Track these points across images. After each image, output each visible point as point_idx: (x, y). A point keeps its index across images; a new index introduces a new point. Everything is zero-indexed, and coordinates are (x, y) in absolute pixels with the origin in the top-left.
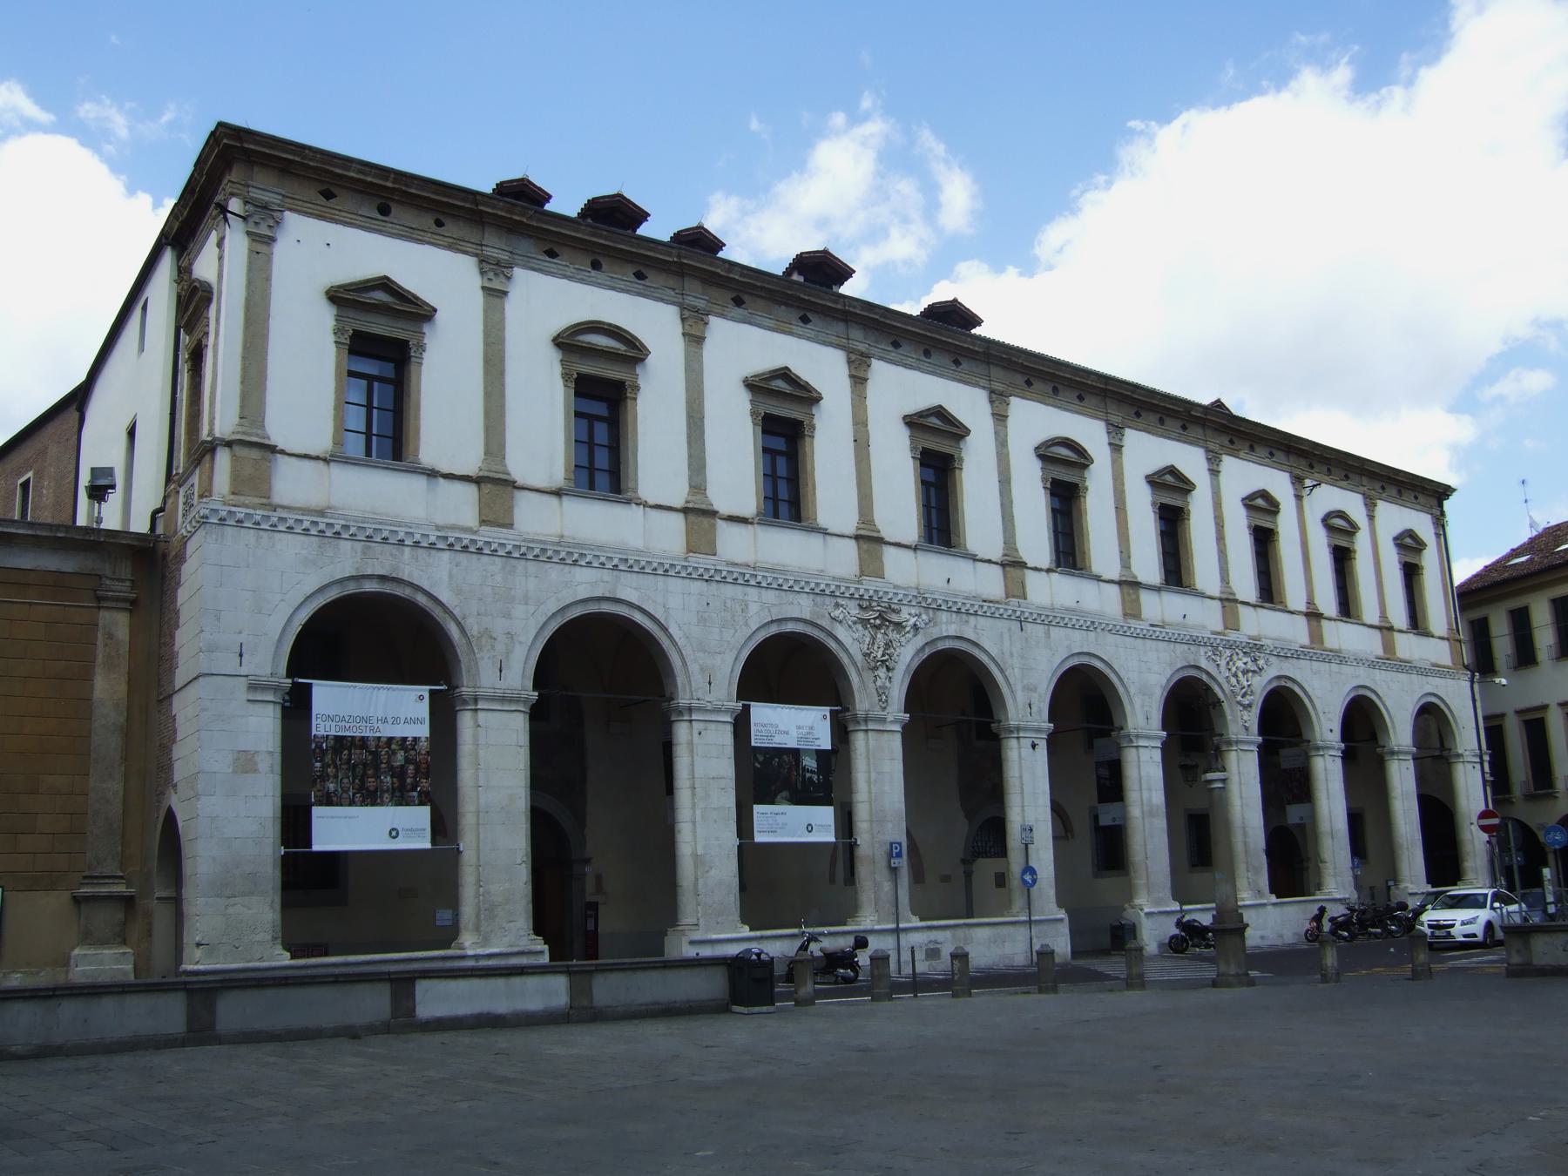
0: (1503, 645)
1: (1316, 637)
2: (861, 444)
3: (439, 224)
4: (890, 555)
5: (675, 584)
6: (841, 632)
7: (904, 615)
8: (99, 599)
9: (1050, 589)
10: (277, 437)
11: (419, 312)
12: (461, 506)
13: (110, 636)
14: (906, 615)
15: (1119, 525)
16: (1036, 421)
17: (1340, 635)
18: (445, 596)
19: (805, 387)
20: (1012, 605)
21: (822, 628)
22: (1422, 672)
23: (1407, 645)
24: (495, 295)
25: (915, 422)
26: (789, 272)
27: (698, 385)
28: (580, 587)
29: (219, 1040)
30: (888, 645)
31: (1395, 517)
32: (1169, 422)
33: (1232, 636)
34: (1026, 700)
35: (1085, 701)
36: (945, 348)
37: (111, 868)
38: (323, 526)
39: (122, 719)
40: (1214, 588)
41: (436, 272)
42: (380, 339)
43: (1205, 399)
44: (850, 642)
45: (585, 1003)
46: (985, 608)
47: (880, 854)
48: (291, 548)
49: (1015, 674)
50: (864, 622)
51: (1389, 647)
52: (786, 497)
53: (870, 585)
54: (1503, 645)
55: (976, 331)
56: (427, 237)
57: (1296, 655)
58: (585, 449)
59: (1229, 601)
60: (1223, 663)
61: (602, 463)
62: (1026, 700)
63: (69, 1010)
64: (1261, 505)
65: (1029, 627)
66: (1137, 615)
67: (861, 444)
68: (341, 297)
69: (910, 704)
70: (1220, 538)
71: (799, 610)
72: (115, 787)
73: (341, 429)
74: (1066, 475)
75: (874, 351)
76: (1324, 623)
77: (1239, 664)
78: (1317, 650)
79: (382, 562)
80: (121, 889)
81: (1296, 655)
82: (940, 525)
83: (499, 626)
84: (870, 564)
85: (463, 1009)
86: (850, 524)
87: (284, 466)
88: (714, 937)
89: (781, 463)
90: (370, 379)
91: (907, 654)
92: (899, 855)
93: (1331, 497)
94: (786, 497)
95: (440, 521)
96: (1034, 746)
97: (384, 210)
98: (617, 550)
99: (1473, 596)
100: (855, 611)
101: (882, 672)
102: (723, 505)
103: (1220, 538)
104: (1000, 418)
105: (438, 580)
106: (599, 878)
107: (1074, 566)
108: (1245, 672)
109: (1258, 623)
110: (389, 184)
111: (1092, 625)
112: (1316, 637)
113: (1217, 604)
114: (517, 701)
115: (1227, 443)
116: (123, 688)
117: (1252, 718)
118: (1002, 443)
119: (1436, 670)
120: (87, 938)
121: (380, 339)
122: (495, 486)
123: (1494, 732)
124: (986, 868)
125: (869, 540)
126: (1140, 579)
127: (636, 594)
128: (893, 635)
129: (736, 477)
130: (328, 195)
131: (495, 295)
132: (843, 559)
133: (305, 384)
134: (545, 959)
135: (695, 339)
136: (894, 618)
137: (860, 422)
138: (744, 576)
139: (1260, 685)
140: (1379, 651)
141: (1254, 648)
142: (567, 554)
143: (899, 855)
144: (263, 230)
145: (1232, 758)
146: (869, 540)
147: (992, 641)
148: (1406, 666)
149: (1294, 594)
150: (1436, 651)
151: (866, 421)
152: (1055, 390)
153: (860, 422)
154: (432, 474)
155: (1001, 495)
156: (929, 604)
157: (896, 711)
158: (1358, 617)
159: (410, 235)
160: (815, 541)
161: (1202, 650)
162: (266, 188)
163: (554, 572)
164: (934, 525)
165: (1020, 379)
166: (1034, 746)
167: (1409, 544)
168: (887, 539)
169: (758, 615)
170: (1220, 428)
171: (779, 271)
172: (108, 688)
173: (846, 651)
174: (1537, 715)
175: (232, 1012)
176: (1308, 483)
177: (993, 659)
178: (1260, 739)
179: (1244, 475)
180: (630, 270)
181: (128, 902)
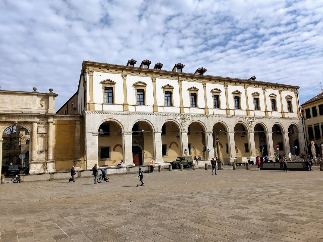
3: (116, 70)
5: (152, 116)
6: (177, 121)
7: (187, 117)
8: (75, 123)
11: (113, 83)
13: (77, 128)
16: (211, 86)
17: (275, 114)
19: (172, 87)
20: (206, 114)
21: (174, 120)
22: (291, 119)
24: (124, 79)
26: (155, 68)
30: (185, 122)
31: (285, 93)
32: (256, 85)
33: (248, 116)
34: (269, 129)
35: (277, 128)
36: (252, 83)
38: (102, 112)
39: (79, 138)
42: (109, 88)
43: (87, 61)
44: (179, 122)
45: (129, 171)
46: (202, 115)
49: (206, 125)
50: (181, 119)
55: (255, 80)
56: (98, 71)
57: (263, 118)
58: (166, 101)
60: (246, 120)
61: (142, 101)
62: (269, 129)
65: (209, 118)
66: (230, 114)
71: (171, 118)
72: (79, 147)
73: (104, 100)
75: (183, 80)
77: (250, 120)
78: (266, 117)
79: (111, 117)
83: (127, 124)
85: (113, 173)
88: (159, 163)
90: (108, 93)
91: (188, 123)
92: (187, 151)
93: (271, 91)
94: (217, 105)
95: (118, 111)
96: (210, 135)
97: (108, 70)
98: (144, 112)
100: (180, 118)
101: (184, 126)
105: (118, 118)
106: (146, 155)
107: (275, 111)
108: (251, 122)
110: (108, 66)
111: (259, 118)
113: (281, 113)
114: (130, 133)
115: (254, 85)
116: (79, 135)
121: (109, 88)
122: (206, 109)
125: (266, 111)
126: (184, 106)
127: (146, 118)
128: (186, 120)
129: (232, 105)
130: (133, 73)
131: (124, 79)
134: (134, 166)
135: (180, 84)
136: (186, 118)
139: (254, 124)
140: (281, 116)
141: (254, 117)
143: (187, 151)
144: (91, 74)
147: (202, 120)
149: (279, 108)
150: (296, 116)
152: (215, 81)
154: (117, 105)
155: (205, 98)
158: (260, 110)
161: (242, 119)
162: (91, 68)
163: (134, 116)
164: (237, 106)
166: (210, 135)
167: (289, 98)
168: (129, 104)
170: (252, 82)
171: (126, 65)
172: (77, 134)
173: (178, 123)
174: (317, 125)
176: (266, 89)
177: (146, 120)
178: (289, 132)
179: (252, 90)
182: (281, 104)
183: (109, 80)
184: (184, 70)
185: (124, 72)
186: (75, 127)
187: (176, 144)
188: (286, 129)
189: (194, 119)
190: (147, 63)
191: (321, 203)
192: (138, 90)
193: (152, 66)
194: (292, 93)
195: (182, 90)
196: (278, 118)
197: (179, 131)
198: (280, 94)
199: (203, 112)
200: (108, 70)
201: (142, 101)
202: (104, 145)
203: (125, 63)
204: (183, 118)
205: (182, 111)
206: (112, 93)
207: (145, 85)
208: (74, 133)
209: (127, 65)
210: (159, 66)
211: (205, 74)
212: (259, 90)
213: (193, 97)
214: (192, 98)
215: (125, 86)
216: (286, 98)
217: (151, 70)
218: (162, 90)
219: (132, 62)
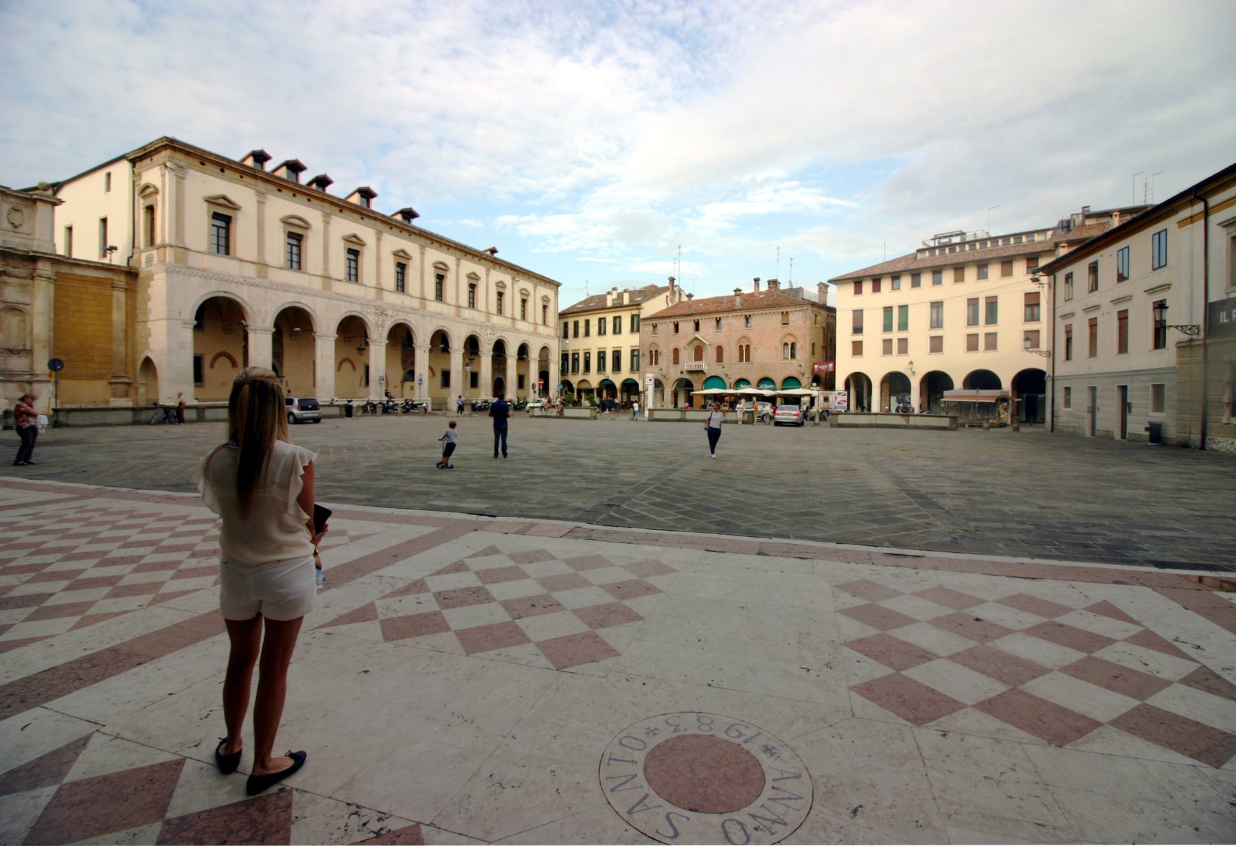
0: (571, 331)
1: (458, 315)
2: (378, 259)
4: (386, 294)
5: (318, 299)
9: (434, 306)
10: (189, 245)
11: (362, 244)
12: (251, 271)
14: (390, 312)
15: (456, 287)
16: (435, 255)
17: (521, 325)
18: (246, 299)
20: (422, 310)
23: (541, 329)
24: (261, 203)
25: (396, 254)
26: (310, 184)
27: (328, 235)
28: (288, 300)
29: (207, 421)
31: (543, 291)
37: (121, 374)
38: (205, 274)
40: (373, 283)
41: (241, 193)
44: (371, 319)
47: (377, 380)
48: (195, 281)
51: (535, 329)
52: (354, 274)
53: (378, 303)
54: (571, 331)
59: (488, 314)
61: (296, 260)
63: (107, 414)
64: (524, 293)
66: (330, 289)
67: (378, 259)
68: (210, 201)
69: (276, 325)
70: (457, 284)
71: (356, 310)
74: (441, 273)
76: (320, 273)
78: (535, 333)
80: (126, 380)
81: (316, 295)
82: (401, 286)
84: (379, 297)
86: (418, 294)
87: (191, 256)
89: (295, 250)
91: (389, 324)
93: (524, 284)
99: (563, 315)
102: (334, 275)
103: (457, 284)
104: (422, 254)
105: (242, 294)
109: (496, 320)
111: (402, 309)
112: (514, 325)
116: (123, 317)
117: (491, 347)
118: (422, 262)
119: (549, 336)
120: (115, 395)
123: (565, 357)
124: (408, 384)
127: (306, 302)
130: (203, 164)
132: (371, 294)
133: (199, 229)
137: (378, 253)
138: (340, 297)
141: (493, 328)
142: (287, 288)
145: (373, 348)
146: (379, 289)
147: (414, 322)
148: (539, 335)
149: (530, 317)
150: (551, 332)
151: (381, 250)
153: (378, 253)
154: (241, 260)
155: (421, 278)
156: (395, 308)
157: (385, 341)
159: (232, 180)
160: (362, 288)
165: (196, 162)
167: (546, 299)
169: (344, 311)
170: (489, 258)
172: (118, 316)
175: (209, 414)
179: (497, 275)
180: (306, 198)
181: (129, 384)
182: (534, 307)
183: (224, 198)
184: (330, 190)
185: (261, 186)
186: (111, 296)
187: (352, 363)
188: (534, 354)
189: (401, 318)
190: (295, 167)
191: (1096, 517)
192: (291, 235)
193: (304, 178)
194: (550, 293)
195: (381, 250)
196: (526, 333)
197: (366, 336)
198: (458, 265)
199: (416, 304)
200: (222, 171)
201: (296, 260)
202: (445, 390)
203: (236, 154)
204: (382, 313)
205: (376, 298)
206: (299, 247)
207: (306, 226)
208: (109, 311)
209: (244, 159)
210: (323, 182)
211: (415, 222)
212: (506, 278)
213: (352, 257)
214: (292, 245)
215: (262, 217)
216: (469, 277)
217: (301, 186)
218: (342, 243)
219: (260, 157)
